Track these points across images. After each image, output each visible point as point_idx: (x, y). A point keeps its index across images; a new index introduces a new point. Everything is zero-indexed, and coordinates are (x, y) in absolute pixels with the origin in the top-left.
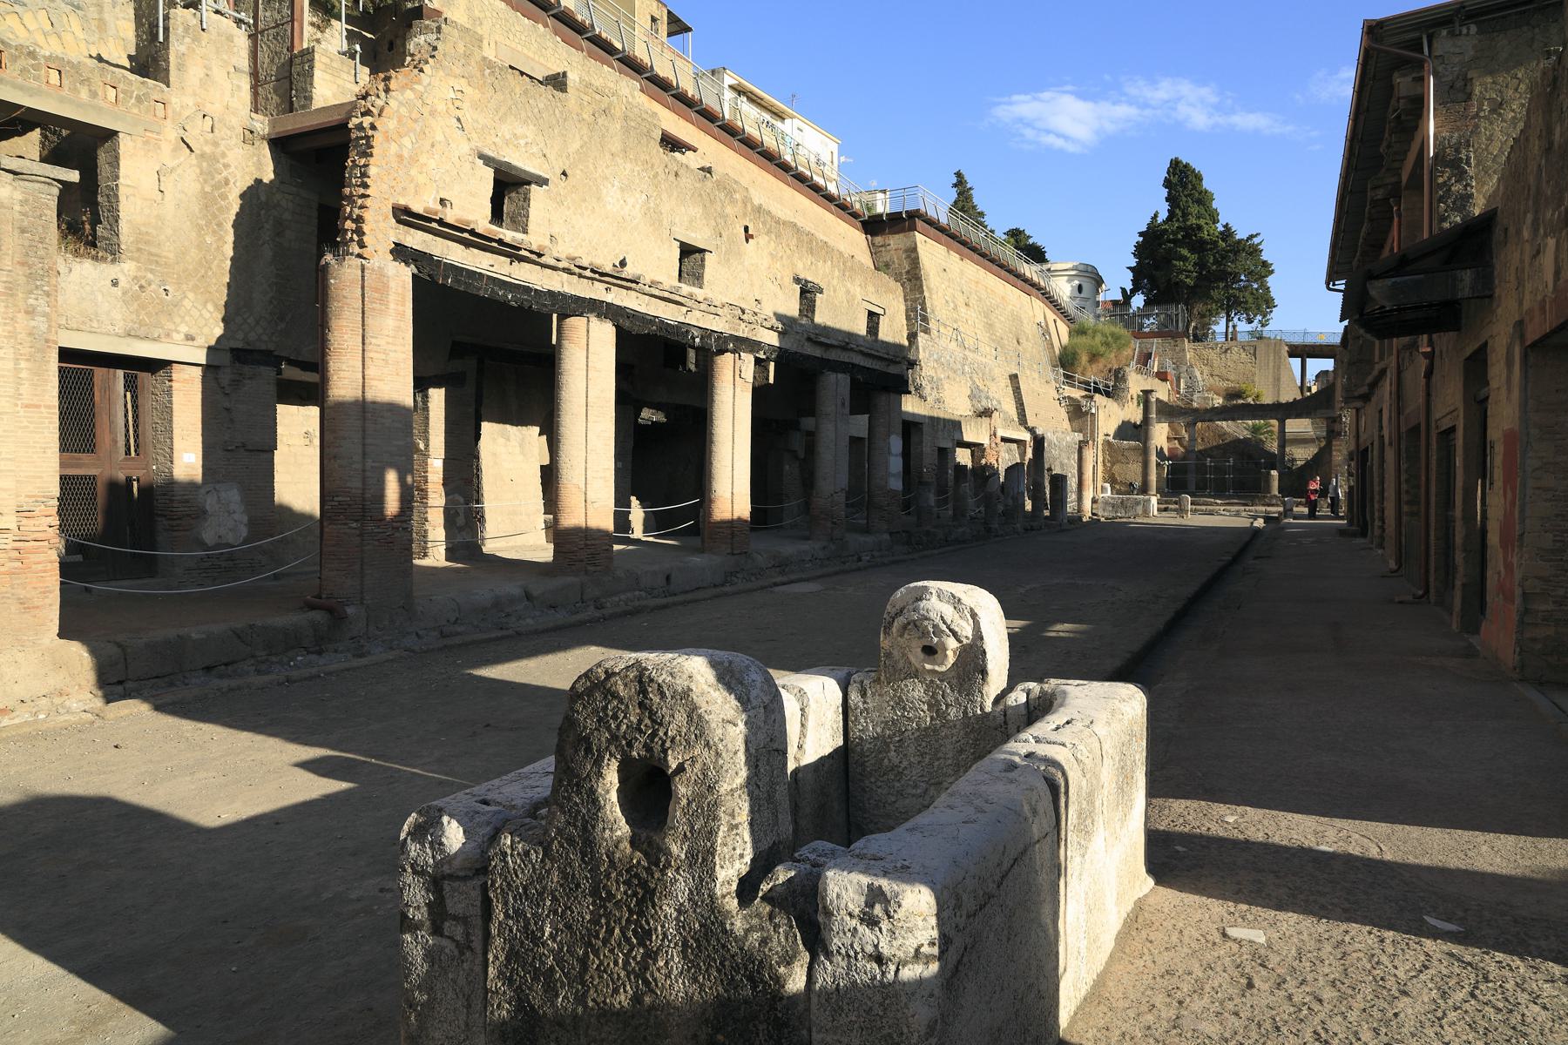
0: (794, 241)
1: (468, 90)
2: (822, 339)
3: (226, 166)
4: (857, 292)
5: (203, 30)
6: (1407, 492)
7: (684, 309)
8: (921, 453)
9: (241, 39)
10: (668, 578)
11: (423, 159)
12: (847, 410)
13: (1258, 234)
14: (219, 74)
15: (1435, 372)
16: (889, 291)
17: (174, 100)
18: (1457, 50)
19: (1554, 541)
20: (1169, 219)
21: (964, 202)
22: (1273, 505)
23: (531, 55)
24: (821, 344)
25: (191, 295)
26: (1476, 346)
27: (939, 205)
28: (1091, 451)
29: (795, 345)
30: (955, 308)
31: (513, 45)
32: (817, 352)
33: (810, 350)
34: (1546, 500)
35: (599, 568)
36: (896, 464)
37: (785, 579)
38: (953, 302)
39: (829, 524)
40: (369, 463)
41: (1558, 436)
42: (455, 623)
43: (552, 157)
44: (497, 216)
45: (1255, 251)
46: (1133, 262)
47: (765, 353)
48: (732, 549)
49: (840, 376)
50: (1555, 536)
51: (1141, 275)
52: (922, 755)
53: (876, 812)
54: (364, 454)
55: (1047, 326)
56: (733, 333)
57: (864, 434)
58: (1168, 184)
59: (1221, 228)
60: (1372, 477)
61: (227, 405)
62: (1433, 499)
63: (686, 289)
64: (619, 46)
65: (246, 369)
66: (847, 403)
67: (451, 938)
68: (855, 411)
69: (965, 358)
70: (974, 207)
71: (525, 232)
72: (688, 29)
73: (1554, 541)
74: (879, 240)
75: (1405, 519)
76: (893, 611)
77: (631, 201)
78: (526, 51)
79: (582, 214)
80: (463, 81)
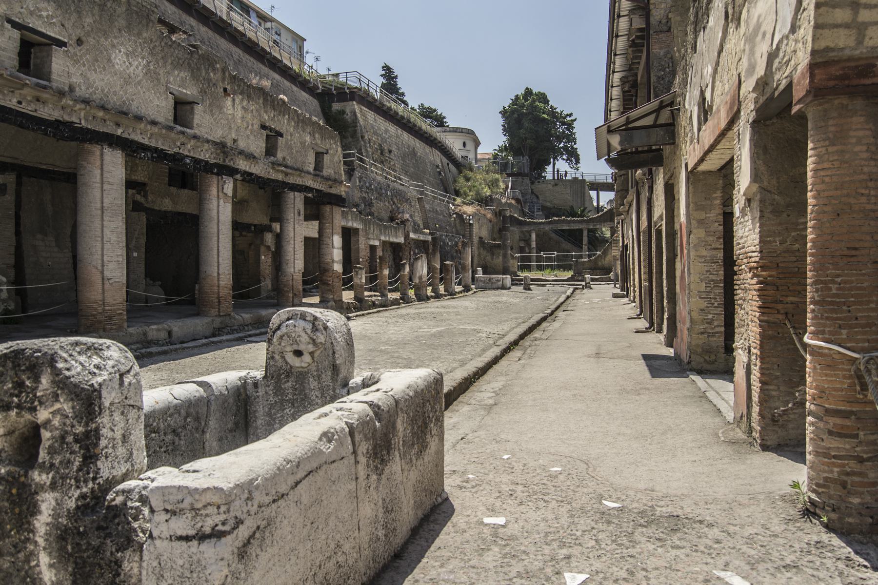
12: (302, 217)
21: (391, 84)
29: (263, 172)
34: (700, 263)
35: (114, 327)
37: (258, 331)
48: (219, 312)
66: (302, 212)
68: (307, 218)
69: (388, 186)
79: (95, 70)
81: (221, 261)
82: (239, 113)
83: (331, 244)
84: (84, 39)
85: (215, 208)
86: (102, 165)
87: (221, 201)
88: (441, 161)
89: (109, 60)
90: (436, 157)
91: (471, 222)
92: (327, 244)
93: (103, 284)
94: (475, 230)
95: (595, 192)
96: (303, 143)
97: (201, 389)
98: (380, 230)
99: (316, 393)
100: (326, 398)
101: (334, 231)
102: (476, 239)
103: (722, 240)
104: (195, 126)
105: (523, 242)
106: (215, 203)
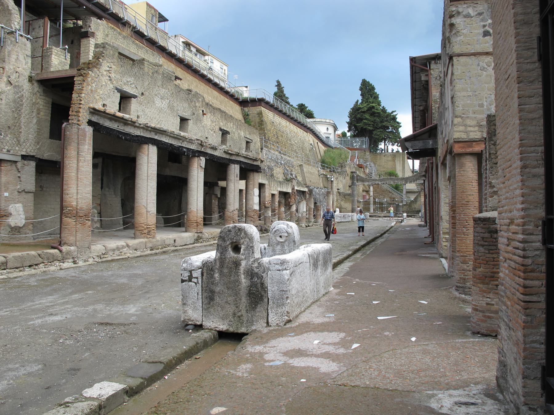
1: (113, 67)
2: (230, 152)
3: (23, 90)
5: (17, 42)
7: (181, 141)
8: (265, 196)
9: (29, 44)
10: (175, 241)
11: (99, 91)
12: (238, 178)
13: (395, 111)
14: (21, 57)
16: (254, 133)
17: (6, 67)
18: (437, 68)
20: (362, 103)
21: (280, 94)
23: (124, 47)
24: (229, 154)
25: (9, 136)
27: (270, 98)
28: (332, 196)
30: (277, 137)
31: (119, 44)
33: (225, 156)
36: (256, 200)
40: (79, 196)
42: (104, 254)
43: (139, 88)
44: (120, 110)
45: (394, 118)
46: (348, 120)
54: (77, 193)
55: (314, 144)
58: (361, 89)
61: (19, 175)
64: (146, 34)
65: (26, 162)
66: (238, 176)
67: (194, 282)
68: (241, 179)
70: (284, 95)
71: (130, 115)
72: (167, 20)
74: (246, 109)
76: (272, 228)
77: (164, 103)
78: (123, 45)
80: (111, 64)
84: (144, 93)
85: (196, 175)
86: (148, 154)
87: (199, 171)
88: (313, 141)
89: (154, 102)
90: (310, 138)
91: (332, 180)
92: (251, 194)
93: (147, 214)
94: (335, 184)
96: (240, 137)
98: (278, 185)
102: (335, 190)
105: (365, 192)
106: (196, 172)
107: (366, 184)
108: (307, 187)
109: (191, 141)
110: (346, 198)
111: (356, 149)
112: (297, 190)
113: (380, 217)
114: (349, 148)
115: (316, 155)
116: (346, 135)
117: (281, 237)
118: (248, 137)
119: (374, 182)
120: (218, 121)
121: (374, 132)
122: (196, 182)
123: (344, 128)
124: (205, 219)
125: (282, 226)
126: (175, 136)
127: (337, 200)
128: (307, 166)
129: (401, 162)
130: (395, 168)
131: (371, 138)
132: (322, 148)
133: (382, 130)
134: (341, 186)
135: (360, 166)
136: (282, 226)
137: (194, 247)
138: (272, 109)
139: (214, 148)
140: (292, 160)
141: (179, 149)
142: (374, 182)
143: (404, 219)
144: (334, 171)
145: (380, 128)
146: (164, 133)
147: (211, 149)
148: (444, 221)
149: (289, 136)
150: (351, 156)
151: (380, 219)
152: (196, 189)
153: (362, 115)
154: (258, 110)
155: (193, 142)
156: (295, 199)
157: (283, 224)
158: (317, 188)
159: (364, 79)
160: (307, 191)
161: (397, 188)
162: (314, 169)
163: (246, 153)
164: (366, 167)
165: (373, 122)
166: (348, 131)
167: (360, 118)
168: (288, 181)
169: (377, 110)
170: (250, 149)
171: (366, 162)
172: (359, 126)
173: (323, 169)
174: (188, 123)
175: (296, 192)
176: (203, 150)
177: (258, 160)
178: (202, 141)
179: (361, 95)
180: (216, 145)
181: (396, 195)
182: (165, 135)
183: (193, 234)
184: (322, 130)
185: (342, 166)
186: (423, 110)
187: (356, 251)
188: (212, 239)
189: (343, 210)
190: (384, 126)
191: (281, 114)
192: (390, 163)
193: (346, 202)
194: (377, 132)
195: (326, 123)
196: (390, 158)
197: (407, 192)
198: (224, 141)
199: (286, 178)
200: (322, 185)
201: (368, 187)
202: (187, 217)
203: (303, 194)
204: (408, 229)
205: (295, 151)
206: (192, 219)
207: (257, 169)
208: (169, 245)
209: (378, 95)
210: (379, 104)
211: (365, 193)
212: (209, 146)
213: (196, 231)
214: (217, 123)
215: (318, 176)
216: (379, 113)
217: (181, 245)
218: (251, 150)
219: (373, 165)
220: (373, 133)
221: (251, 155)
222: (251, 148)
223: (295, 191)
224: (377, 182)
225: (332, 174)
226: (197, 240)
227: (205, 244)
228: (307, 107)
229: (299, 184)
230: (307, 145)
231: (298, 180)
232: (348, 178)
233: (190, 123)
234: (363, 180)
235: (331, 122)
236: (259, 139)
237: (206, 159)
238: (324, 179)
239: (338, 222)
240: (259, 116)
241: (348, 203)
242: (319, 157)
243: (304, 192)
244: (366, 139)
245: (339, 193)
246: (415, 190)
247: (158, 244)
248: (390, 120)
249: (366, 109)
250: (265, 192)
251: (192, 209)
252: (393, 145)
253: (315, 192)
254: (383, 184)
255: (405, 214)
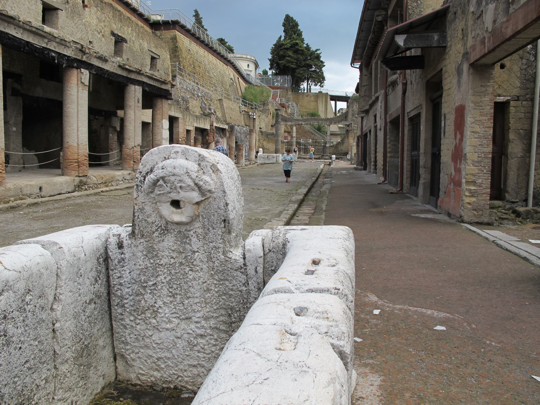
0: (111, 14)
2: (127, 67)
4: (146, 45)
6: (389, 147)
7: (46, 40)
8: (178, 132)
10: (41, 189)
12: (140, 105)
13: (319, 49)
15: (407, 91)
16: (162, 47)
19: (478, 157)
22: (327, 159)
26: (435, 73)
30: (194, 68)
32: (124, 74)
33: (120, 72)
34: (475, 138)
37: (107, 189)
38: (194, 65)
39: (132, 162)
41: (481, 108)
45: (318, 57)
46: (270, 57)
47: (95, 71)
48: (79, 173)
49: (137, 87)
50: (479, 155)
51: (273, 63)
52: (174, 296)
53: (136, 344)
56: (76, 57)
57: (150, 121)
58: (284, 25)
59: (305, 45)
60: (370, 144)
62: (406, 148)
63: (47, 29)
68: (144, 107)
73: (478, 157)
75: (388, 159)
81: (80, 135)
82: (95, 21)
83: (161, 126)
85: (76, 94)
87: (80, 89)
88: (234, 76)
90: (231, 73)
91: (255, 117)
94: (257, 123)
95: (334, 102)
96: (142, 49)
97: (47, 253)
98: (194, 120)
99: (201, 256)
100: (214, 263)
101: (164, 117)
103: (492, 121)
104: (60, 28)
105: (287, 133)
106: (76, 90)
107: (289, 123)
108: (227, 124)
109: (62, 42)
110: (268, 138)
111: (277, 88)
112: (216, 127)
113: (305, 158)
114: (270, 87)
115: (237, 91)
116: (267, 74)
117: (176, 204)
118: (154, 51)
119: (297, 123)
120: (108, 21)
121: (297, 71)
122: (76, 104)
123: (265, 65)
124: (91, 158)
125: (181, 161)
126: (34, 29)
127: (259, 140)
128: (228, 101)
129: (324, 103)
130: (318, 109)
131: (293, 77)
132: (243, 84)
133: (305, 69)
134: (263, 125)
135: (283, 106)
136: (181, 161)
137: (69, 198)
138: (189, 35)
139: (104, 60)
140: (210, 92)
141: (43, 53)
142: (297, 123)
143: (332, 162)
144: (255, 108)
145: (303, 66)
146: (11, 20)
147: (99, 60)
148: (469, 162)
149: (208, 67)
150: (273, 95)
151: (306, 161)
152: (76, 114)
153: (285, 52)
154: (172, 34)
155: (68, 44)
156: (213, 137)
157: (185, 155)
158: (238, 126)
159: (288, 15)
160: (227, 128)
161: (319, 129)
162: (235, 105)
163: (151, 72)
164: (288, 107)
165: (296, 59)
166: (270, 69)
167: (282, 55)
168: (206, 116)
169: (300, 47)
170: (156, 68)
171: (288, 101)
172: (282, 63)
173: (244, 105)
174: (57, 14)
175: (215, 130)
176: (84, 59)
177: (167, 84)
178: (82, 46)
179: (284, 31)
180: (106, 55)
181: (318, 136)
182: (14, 25)
183: (72, 178)
184: (243, 66)
185: (264, 104)
186: (381, 22)
187: (301, 203)
188: (102, 185)
189: (265, 151)
190: (308, 64)
191: (199, 42)
192: (313, 104)
193: (268, 142)
194: (300, 71)
195: (246, 59)
196: (312, 99)
197: (331, 134)
198: (118, 51)
199: (204, 113)
200: (243, 123)
201: (289, 128)
202: (64, 155)
203: (223, 132)
204: (344, 172)
205: (214, 85)
206: (71, 158)
207: (166, 95)
208: (30, 196)
209: (302, 32)
210: (303, 40)
211: (286, 134)
212: (95, 54)
213: (77, 174)
214: (106, 24)
215: (239, 112)
216: (302, 50)
217: (52, 194)
218: (158, 68)
219: (295, 105)
220: (295, 72)
221: (157, 75)
222: (158, 66)
223: (214, 128)
224: (300, 123)
225: (255, 111)
226: (79, 186)
227: (92, 191)
228: (227, 42)
229: (218, 120)
230: (226, 79)
231: (217, 116)
232: (270, 117)
233: (62, 15)
234: (285, 120)
235: (252, 58)
236: (169, 56)
237: (90, 73)
238: (246, 116)
239: (261, 164)
240: (173, 41)
241: (271, 144)
242: (240, 94)
243: (223, 130)
244: (288, 78)
245: (261, 132)
246: (337, 133)
247: (9, 194)
248: (314, 58)
249: (289, 45)
250: (178, 127)
251: (71, 143)
252: (316, 85)
253: (237, 131)
254: (307, 124)
255: (334, 156)
